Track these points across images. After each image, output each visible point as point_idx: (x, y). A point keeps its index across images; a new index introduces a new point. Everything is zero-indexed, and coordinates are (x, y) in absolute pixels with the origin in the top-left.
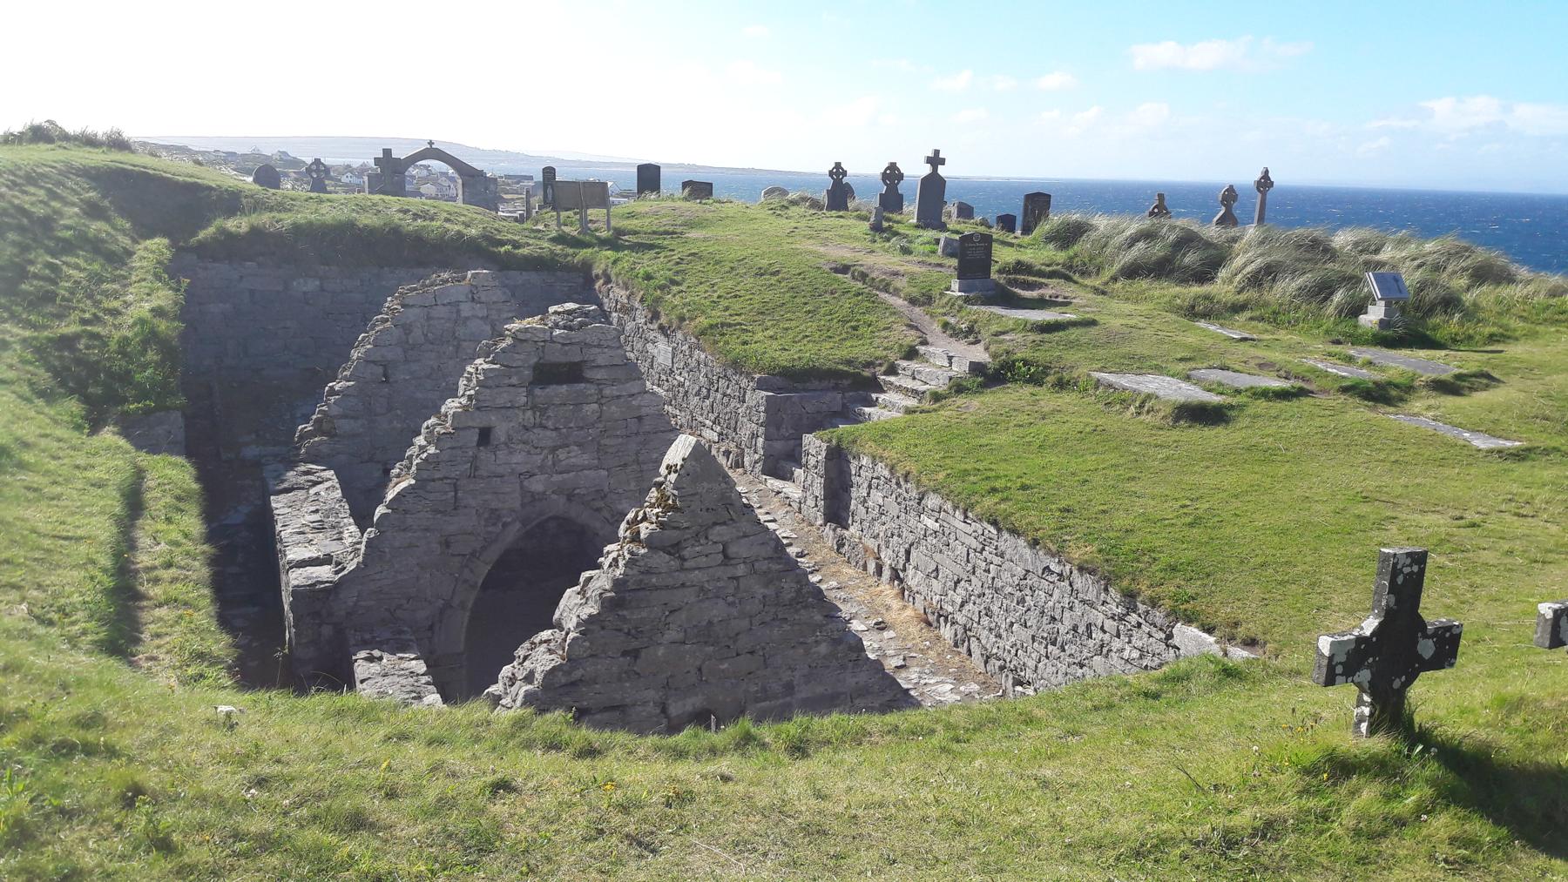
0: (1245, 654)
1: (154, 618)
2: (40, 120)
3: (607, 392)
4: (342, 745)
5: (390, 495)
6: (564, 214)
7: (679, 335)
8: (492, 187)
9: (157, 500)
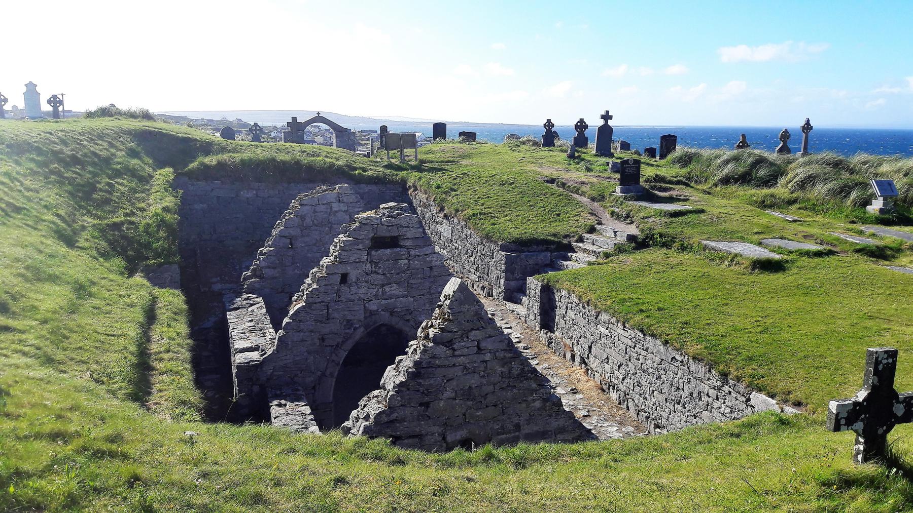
0: (795, 411)
1: (159, 381)
2: (105, 104)
3: (412, 253)
4: (253, 455)
5: (291, 312)
6: (391, 152)
7: (456, 220)
8: (352, 138)
9: (163, 314)
